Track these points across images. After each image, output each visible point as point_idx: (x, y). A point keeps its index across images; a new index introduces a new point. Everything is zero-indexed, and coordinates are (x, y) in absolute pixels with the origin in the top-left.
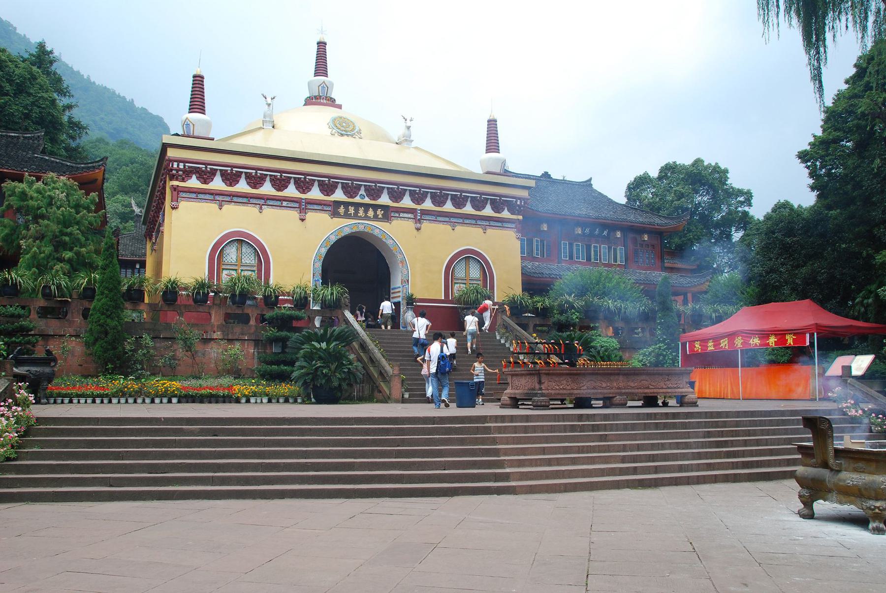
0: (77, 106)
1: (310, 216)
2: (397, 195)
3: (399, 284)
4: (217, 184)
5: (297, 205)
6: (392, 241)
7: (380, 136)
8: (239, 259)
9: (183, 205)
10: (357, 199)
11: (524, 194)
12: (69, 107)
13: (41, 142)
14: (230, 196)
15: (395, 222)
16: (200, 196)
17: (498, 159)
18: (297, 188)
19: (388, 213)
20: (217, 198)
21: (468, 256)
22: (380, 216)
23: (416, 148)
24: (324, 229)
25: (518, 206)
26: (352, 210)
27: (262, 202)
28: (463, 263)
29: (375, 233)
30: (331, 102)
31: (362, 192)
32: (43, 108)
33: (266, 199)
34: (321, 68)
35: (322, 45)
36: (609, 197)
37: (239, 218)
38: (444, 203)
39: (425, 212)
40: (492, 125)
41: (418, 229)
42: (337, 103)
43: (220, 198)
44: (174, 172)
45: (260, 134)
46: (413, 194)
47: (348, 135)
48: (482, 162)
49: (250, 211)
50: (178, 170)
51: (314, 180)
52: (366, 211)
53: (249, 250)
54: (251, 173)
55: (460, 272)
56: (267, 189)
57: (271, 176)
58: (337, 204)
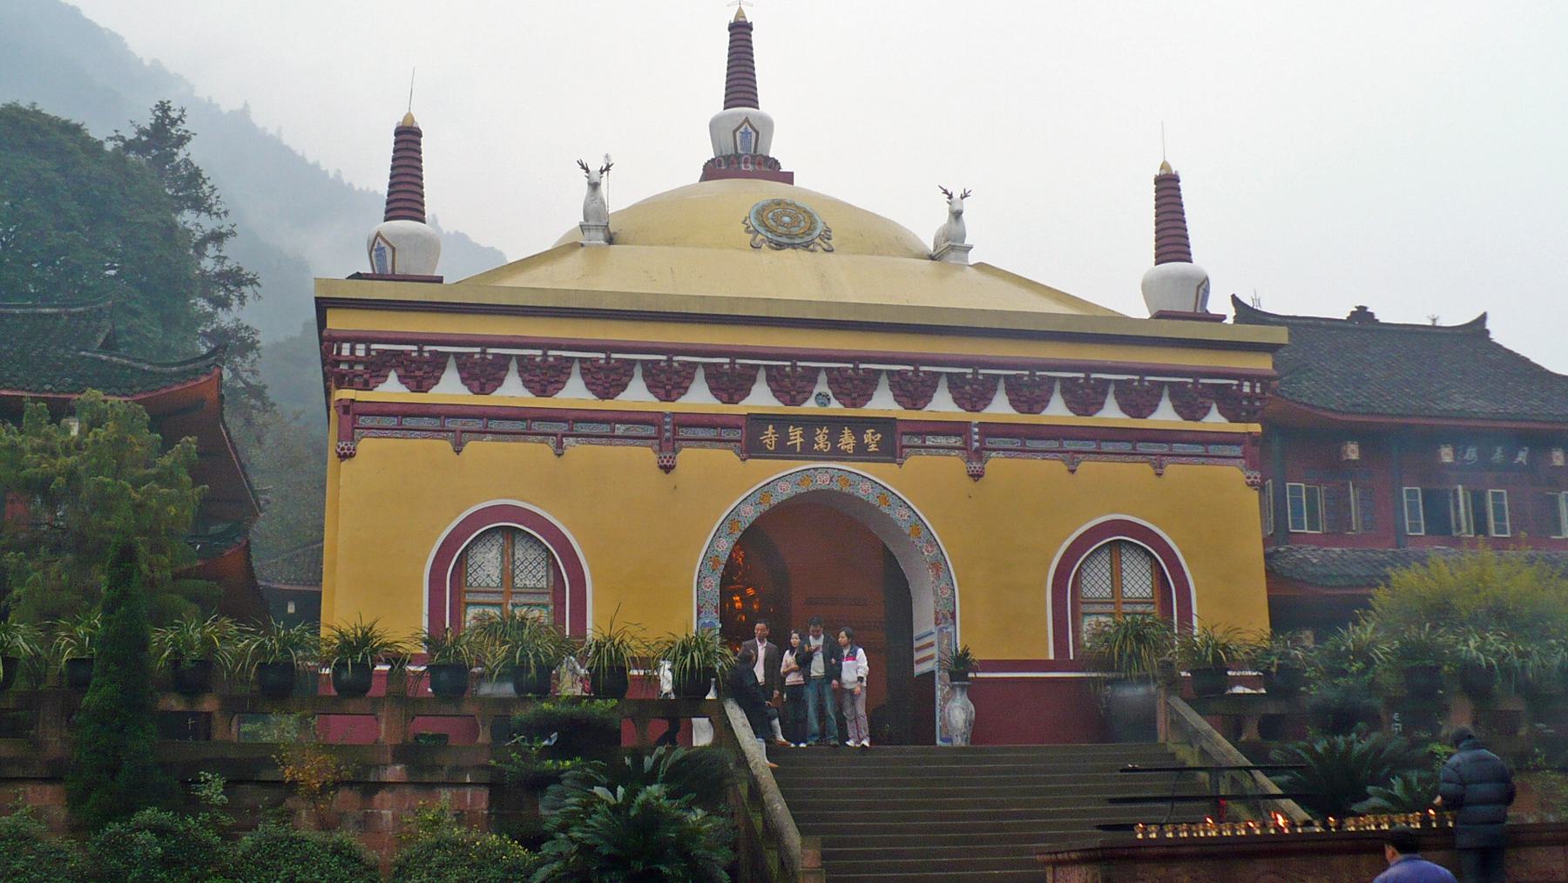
0: (233, 234)
1: (688, 457)
2: (913, 391)
3: (932, 627)
4: (450, 389)
5: (651, 431)
6: (904, 511)
7: (882, 240)
8: (508, 575)
9: (367, 446)
10: (810, 407)
11: (1263, 363)
12: (218, 237)
13: (104, 322)
14: (481, 418)
15: (914, 462)
16: (409, 422)
17: (1185, 279)
18: (650, 387)
19: (892, 441)
20: (450, 424)
21: (1117, 539)
22: (873, 448)
23: (981, 267)
24: (728, 489)
25: (1247, 396)
26: (796, 436)
27: (563, 428)
28: (1105, 557)
29: (861, 494)
30: (771, 170)
31: (822, 387)
32: (147, 248)
33: (573, 423)
34: (741, 83)
35: (740, 32)
36: (1534, 360)
37: (502, 472)
38: (1043, 402)
39: (989, 430)
40: (1168, 188)
41: (977, 476)
42: (784, 168)
43: (456, 424)
44: (343, 367)
45: (575, 260)
46: (956, 385)
47: (794, 246)
48: (1148, 289)
49: (533, 453)
50: (354, 360)
51: (633, 363)
52: (834, 438)
53: (533, 554)
54: (532, 358)
55: (1097, 583)
56: (575, 394)
57: (582, 360)
58: (758, 421)
